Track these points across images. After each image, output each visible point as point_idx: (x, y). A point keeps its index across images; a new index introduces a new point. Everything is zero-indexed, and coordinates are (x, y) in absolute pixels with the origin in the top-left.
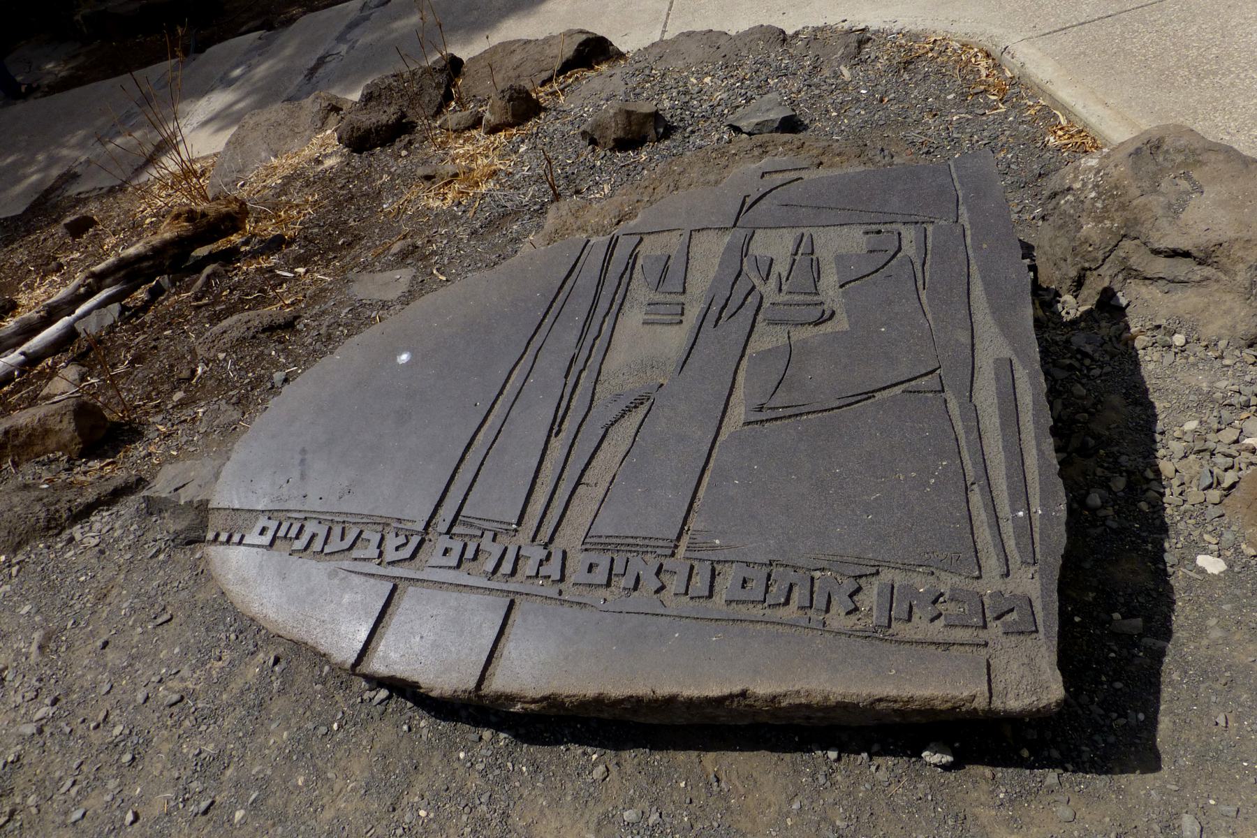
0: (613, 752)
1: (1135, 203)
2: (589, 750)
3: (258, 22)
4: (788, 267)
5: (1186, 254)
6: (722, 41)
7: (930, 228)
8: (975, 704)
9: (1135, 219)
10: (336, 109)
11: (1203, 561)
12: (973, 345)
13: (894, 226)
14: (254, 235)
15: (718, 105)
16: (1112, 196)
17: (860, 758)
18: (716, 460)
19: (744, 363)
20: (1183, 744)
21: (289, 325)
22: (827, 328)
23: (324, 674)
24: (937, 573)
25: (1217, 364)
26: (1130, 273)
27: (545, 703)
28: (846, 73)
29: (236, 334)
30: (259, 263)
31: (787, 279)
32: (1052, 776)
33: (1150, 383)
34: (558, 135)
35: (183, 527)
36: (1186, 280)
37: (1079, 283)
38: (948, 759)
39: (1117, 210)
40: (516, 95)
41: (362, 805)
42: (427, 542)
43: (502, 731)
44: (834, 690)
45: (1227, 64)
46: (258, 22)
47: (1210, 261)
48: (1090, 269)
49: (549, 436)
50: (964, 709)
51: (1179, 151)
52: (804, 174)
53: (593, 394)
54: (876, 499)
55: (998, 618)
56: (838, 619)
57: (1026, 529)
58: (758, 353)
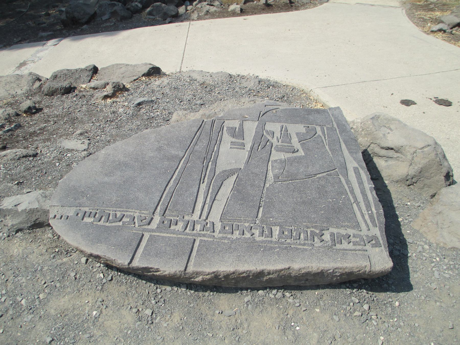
5: (392, 149)
22: (295, 155)
27: (213, 275)
31: (280, 138)
35: (17, 222)
36: (392, 157)
50: (362, 271)
54: (324, 207)
55: (369, 242)
57: (371, 216)
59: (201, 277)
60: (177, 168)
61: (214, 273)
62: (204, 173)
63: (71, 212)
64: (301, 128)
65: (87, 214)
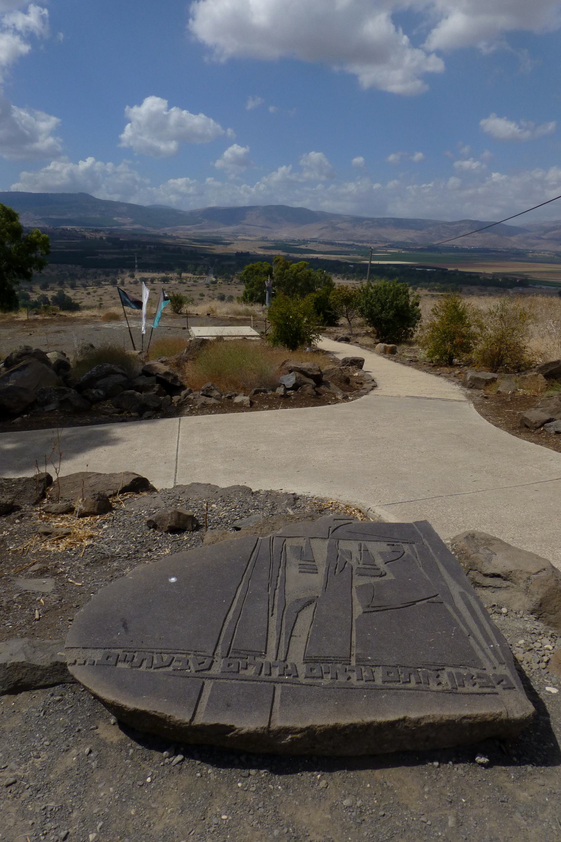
0: (328, 773)
1: (472, 556)
2: (315, 773)
4: (359, 555)
5: (498, 576)
9: (474, 562)
11: (548, 689)
15: (224, 518)
16: (462, 553)
22: (383, 578)
32: (529, 768)
36: (500, 587)
39: (465, 559)
42: (215, 662)
43: (262, 769)
44: (444, 714)
47: (508, 579)
50: (498, 720)
54: (433, 641)
55: (498, 684)
56: (433, 686)
57: (494, 650)
59: (290, 737)
60: (235, 597)
61: (308, 728)
63: (97, 656)
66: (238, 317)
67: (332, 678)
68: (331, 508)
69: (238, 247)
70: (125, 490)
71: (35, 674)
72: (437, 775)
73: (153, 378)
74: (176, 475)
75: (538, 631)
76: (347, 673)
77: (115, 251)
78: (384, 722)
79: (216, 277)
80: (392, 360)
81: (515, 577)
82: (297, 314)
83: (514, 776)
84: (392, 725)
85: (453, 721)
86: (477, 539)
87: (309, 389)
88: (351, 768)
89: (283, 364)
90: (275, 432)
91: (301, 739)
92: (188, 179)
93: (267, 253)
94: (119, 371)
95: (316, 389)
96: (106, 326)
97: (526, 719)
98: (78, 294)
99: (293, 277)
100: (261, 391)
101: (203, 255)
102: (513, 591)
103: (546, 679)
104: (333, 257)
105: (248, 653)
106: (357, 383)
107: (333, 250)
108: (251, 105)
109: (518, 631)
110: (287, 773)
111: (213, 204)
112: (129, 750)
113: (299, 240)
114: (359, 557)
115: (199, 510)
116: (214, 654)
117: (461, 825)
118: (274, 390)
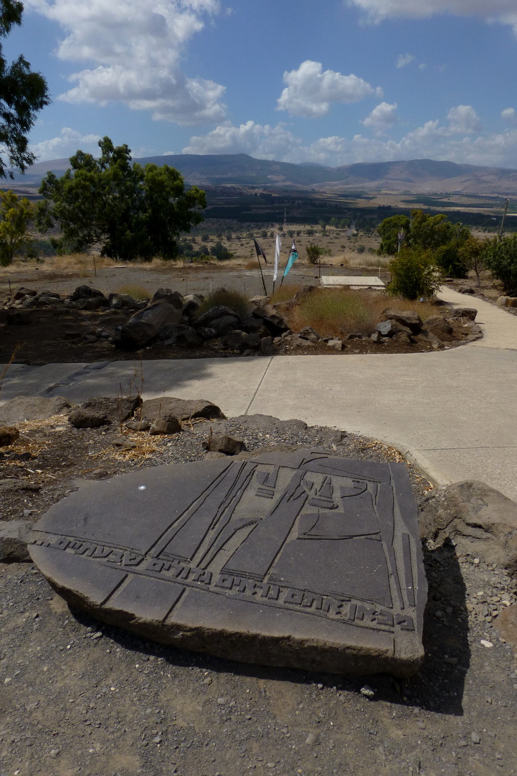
1: (460, 504)
2: (204, 670)
3: (23, 360)
4: (320, 487)
5: (480, 527)
6: (276, 422)
7: (379, 485)
8: (388, 655)
9: (460, 511)
10: (68, 406)
11: (483, 642)
12: (394, 528)
13: (365, 481)
14: (13, 451)
16: (451, 501)
17: (332, 690)
18: (284, 549)
19: (299, 517)
20: (473, 707)
21: (36, 490)
22: (335, 511)
23: (64, 624)
24: (375, 604)
25: (492, 572)
26: (458, 532)
28: (335, 447)
29: (7, 487)
30: (16, 463)
32: (416, 710)
33: (464, 576)
34: (189, 443)
37: (436, 536)
38: (371, 693)
40: (171, 420)
41: (79, 683)
43: (160, 657)
45: (503, 477)
46: (23, 360)
48: (441, 529)
49: (209, 529)
50: (383, 657)
51: (479, 489)
52: (329, 456)
53: (231, 517)
55: (399, 623)
56: (332, 614)
57: (411, 594)
58: (305, 514)
59: (181, 633)
61: (197, 629)
62: (217, 518)
64: (348, 483)
65: (71, 545)
66: (370, 268)
67: (239, 591)
68: (374, 448)
69: (381, 202)
70: (197, 415)
71: (23, 550)
72: (317, 695)
73: (261, 320)
74: (249, 407)
75: (502, 586)
76: (256, 588)
77: (266, 206)
78: (268, 637)
79: (357, 230)
80: (511, 313)
81: (497, 530)
82: (417, 265)
83: (396, 713)
84: (276, 641)
85: (337, 649)
86: (474, 489)
87: (403, 337)
88: (237, 673)
89: (384, 312)
90: (354, 374)
91: (191, 637)
92: (337, 137)
93: (408, 207)
94: (232, 312)
95: (412, 337)
96: (248, 273)
97: (413, 661)
98: (233, 245)
99: (429, 229)
100: (356, 336)
101: (346, 209)
102: (492, 544)
103: (487, 633)
104: (475, 210)
105: (175, 557)
106: (463, 334)
107: (476, 202)
108: (401, 63)
109: (481, 583)
110: (181, 665)
111: (359, 160)
112: (65, 621)
113: (442, 194)
114: (319, 489)
115: (253, 438)
116: (146, 553)
117: (318, 745)
118: (370, 336)
